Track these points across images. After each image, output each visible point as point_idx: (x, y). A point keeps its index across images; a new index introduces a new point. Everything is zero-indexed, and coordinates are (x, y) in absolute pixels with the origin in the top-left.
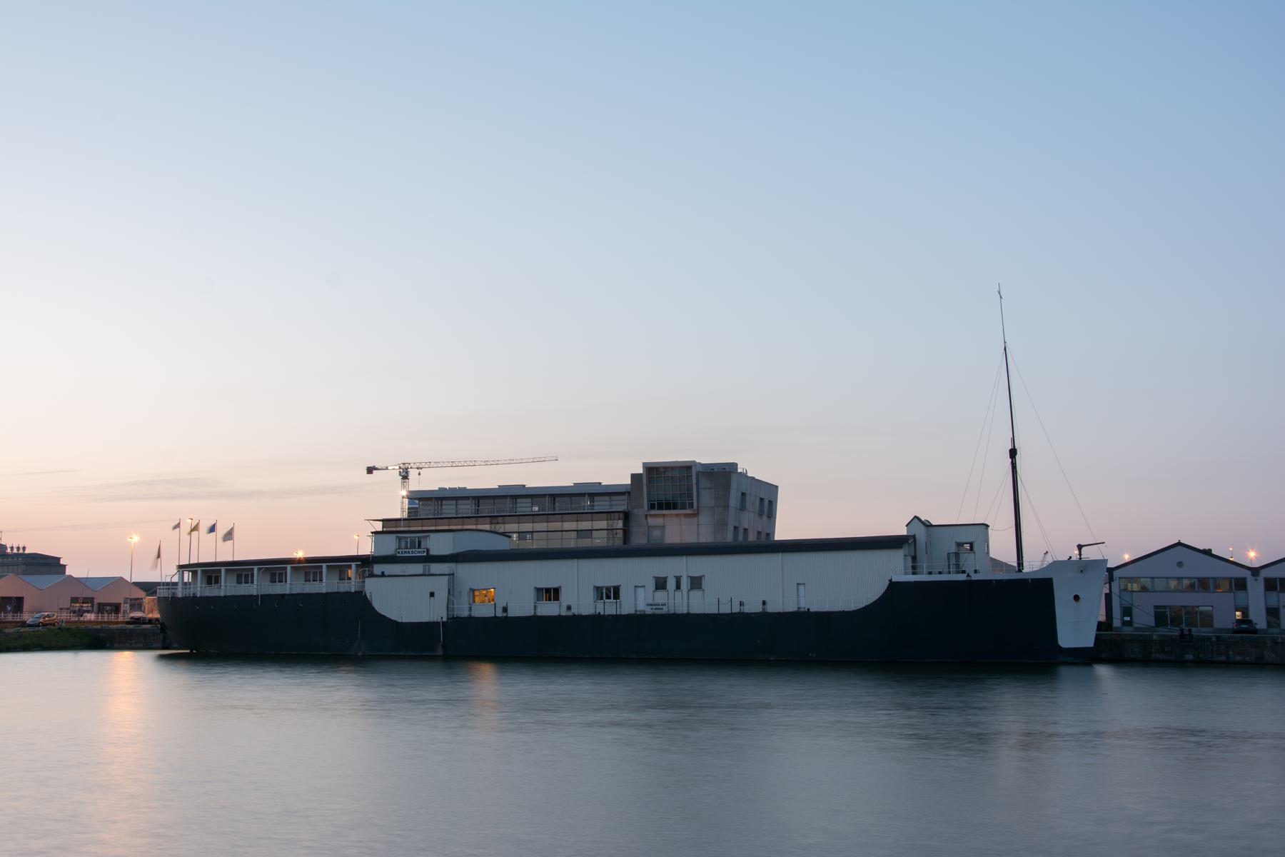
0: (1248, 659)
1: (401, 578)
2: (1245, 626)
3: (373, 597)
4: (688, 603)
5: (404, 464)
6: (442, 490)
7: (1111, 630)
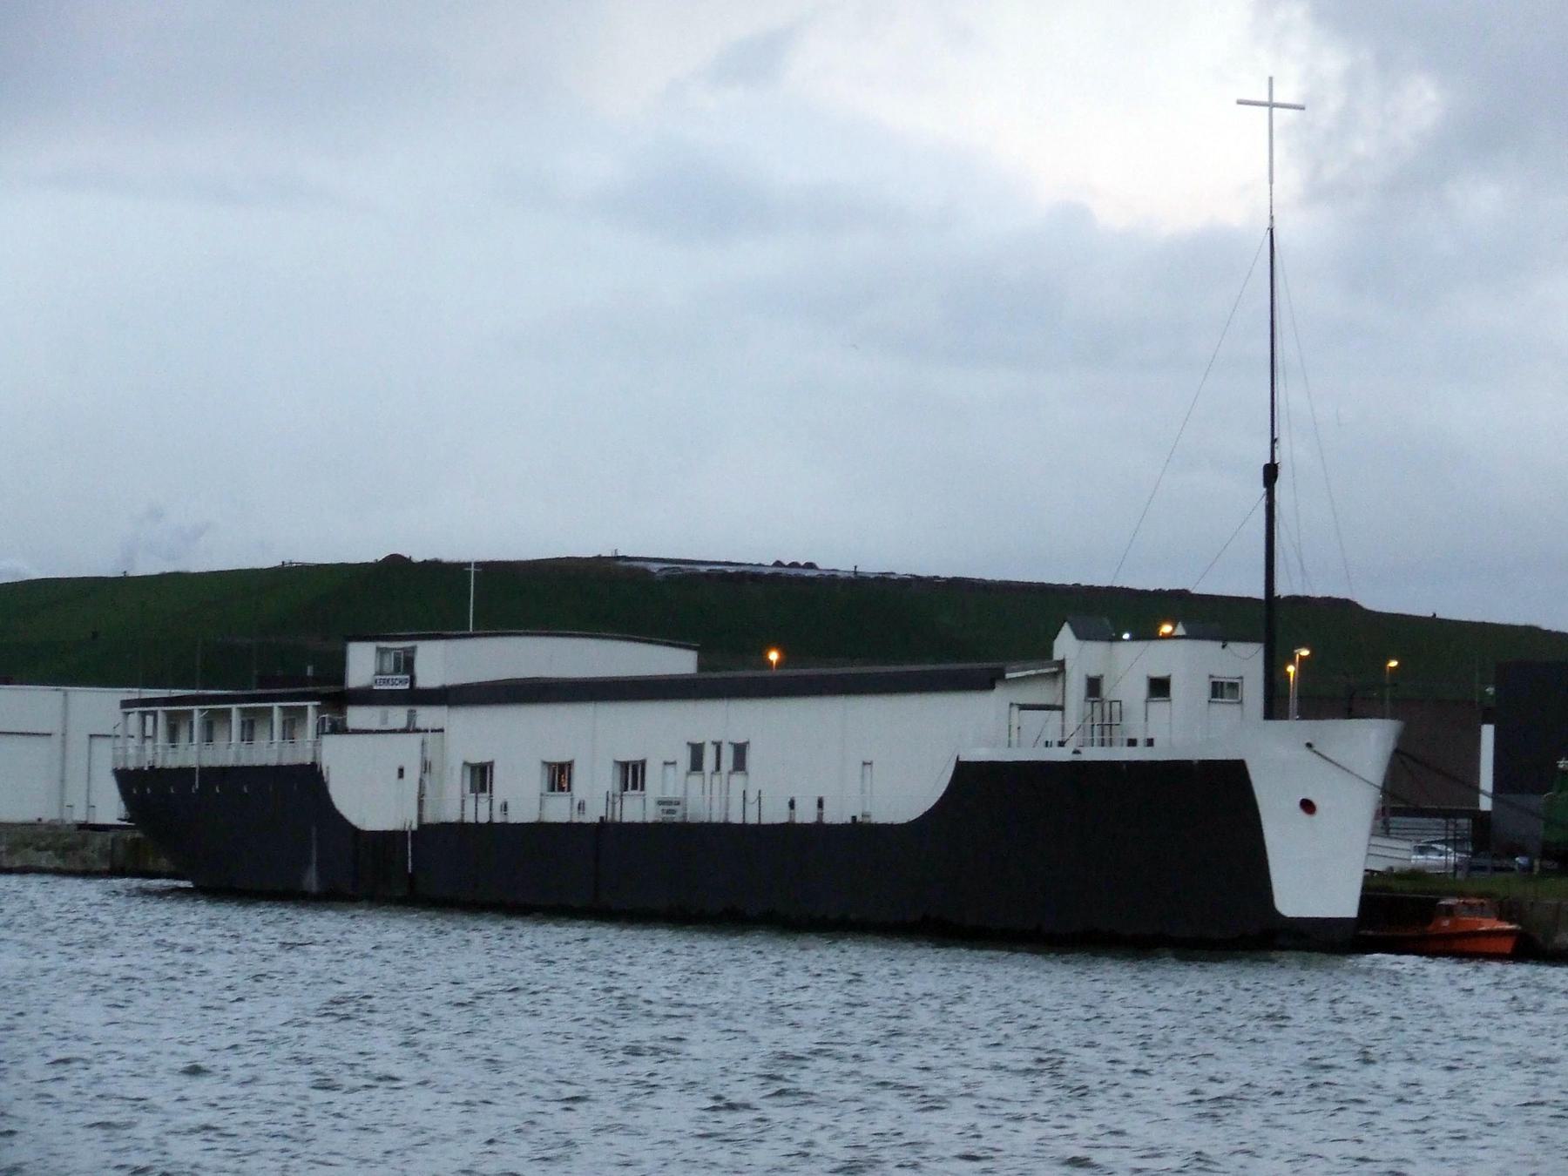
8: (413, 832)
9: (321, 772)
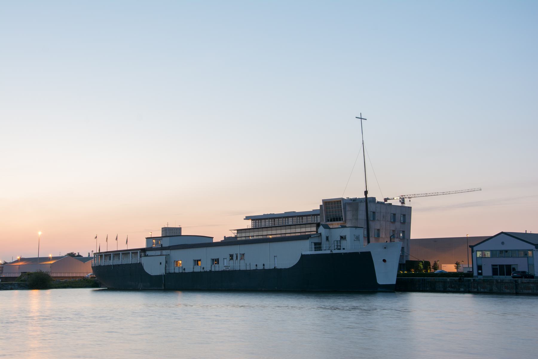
0: (486, 290)
1: (153, 257)
2: (516, 275)
3: (144, 265)
4: (240, 265)
5: (402, 196)
6: (264, 215)
7: (473, 277)
8: (164, 275)
9: (142, 264)
